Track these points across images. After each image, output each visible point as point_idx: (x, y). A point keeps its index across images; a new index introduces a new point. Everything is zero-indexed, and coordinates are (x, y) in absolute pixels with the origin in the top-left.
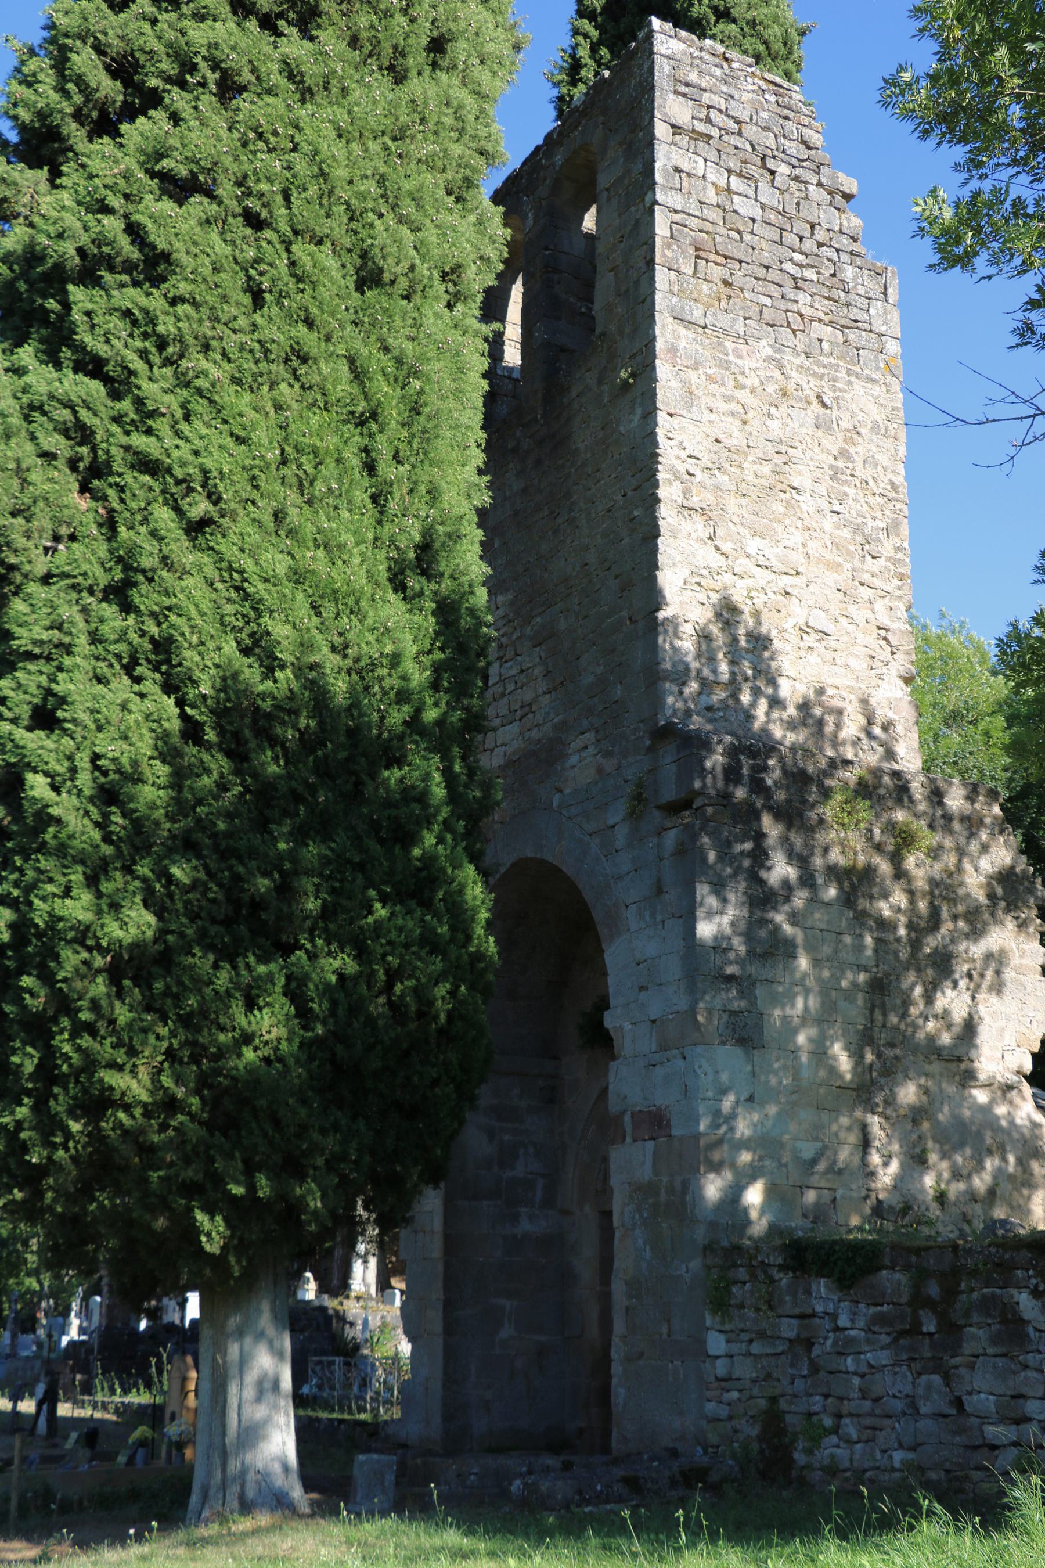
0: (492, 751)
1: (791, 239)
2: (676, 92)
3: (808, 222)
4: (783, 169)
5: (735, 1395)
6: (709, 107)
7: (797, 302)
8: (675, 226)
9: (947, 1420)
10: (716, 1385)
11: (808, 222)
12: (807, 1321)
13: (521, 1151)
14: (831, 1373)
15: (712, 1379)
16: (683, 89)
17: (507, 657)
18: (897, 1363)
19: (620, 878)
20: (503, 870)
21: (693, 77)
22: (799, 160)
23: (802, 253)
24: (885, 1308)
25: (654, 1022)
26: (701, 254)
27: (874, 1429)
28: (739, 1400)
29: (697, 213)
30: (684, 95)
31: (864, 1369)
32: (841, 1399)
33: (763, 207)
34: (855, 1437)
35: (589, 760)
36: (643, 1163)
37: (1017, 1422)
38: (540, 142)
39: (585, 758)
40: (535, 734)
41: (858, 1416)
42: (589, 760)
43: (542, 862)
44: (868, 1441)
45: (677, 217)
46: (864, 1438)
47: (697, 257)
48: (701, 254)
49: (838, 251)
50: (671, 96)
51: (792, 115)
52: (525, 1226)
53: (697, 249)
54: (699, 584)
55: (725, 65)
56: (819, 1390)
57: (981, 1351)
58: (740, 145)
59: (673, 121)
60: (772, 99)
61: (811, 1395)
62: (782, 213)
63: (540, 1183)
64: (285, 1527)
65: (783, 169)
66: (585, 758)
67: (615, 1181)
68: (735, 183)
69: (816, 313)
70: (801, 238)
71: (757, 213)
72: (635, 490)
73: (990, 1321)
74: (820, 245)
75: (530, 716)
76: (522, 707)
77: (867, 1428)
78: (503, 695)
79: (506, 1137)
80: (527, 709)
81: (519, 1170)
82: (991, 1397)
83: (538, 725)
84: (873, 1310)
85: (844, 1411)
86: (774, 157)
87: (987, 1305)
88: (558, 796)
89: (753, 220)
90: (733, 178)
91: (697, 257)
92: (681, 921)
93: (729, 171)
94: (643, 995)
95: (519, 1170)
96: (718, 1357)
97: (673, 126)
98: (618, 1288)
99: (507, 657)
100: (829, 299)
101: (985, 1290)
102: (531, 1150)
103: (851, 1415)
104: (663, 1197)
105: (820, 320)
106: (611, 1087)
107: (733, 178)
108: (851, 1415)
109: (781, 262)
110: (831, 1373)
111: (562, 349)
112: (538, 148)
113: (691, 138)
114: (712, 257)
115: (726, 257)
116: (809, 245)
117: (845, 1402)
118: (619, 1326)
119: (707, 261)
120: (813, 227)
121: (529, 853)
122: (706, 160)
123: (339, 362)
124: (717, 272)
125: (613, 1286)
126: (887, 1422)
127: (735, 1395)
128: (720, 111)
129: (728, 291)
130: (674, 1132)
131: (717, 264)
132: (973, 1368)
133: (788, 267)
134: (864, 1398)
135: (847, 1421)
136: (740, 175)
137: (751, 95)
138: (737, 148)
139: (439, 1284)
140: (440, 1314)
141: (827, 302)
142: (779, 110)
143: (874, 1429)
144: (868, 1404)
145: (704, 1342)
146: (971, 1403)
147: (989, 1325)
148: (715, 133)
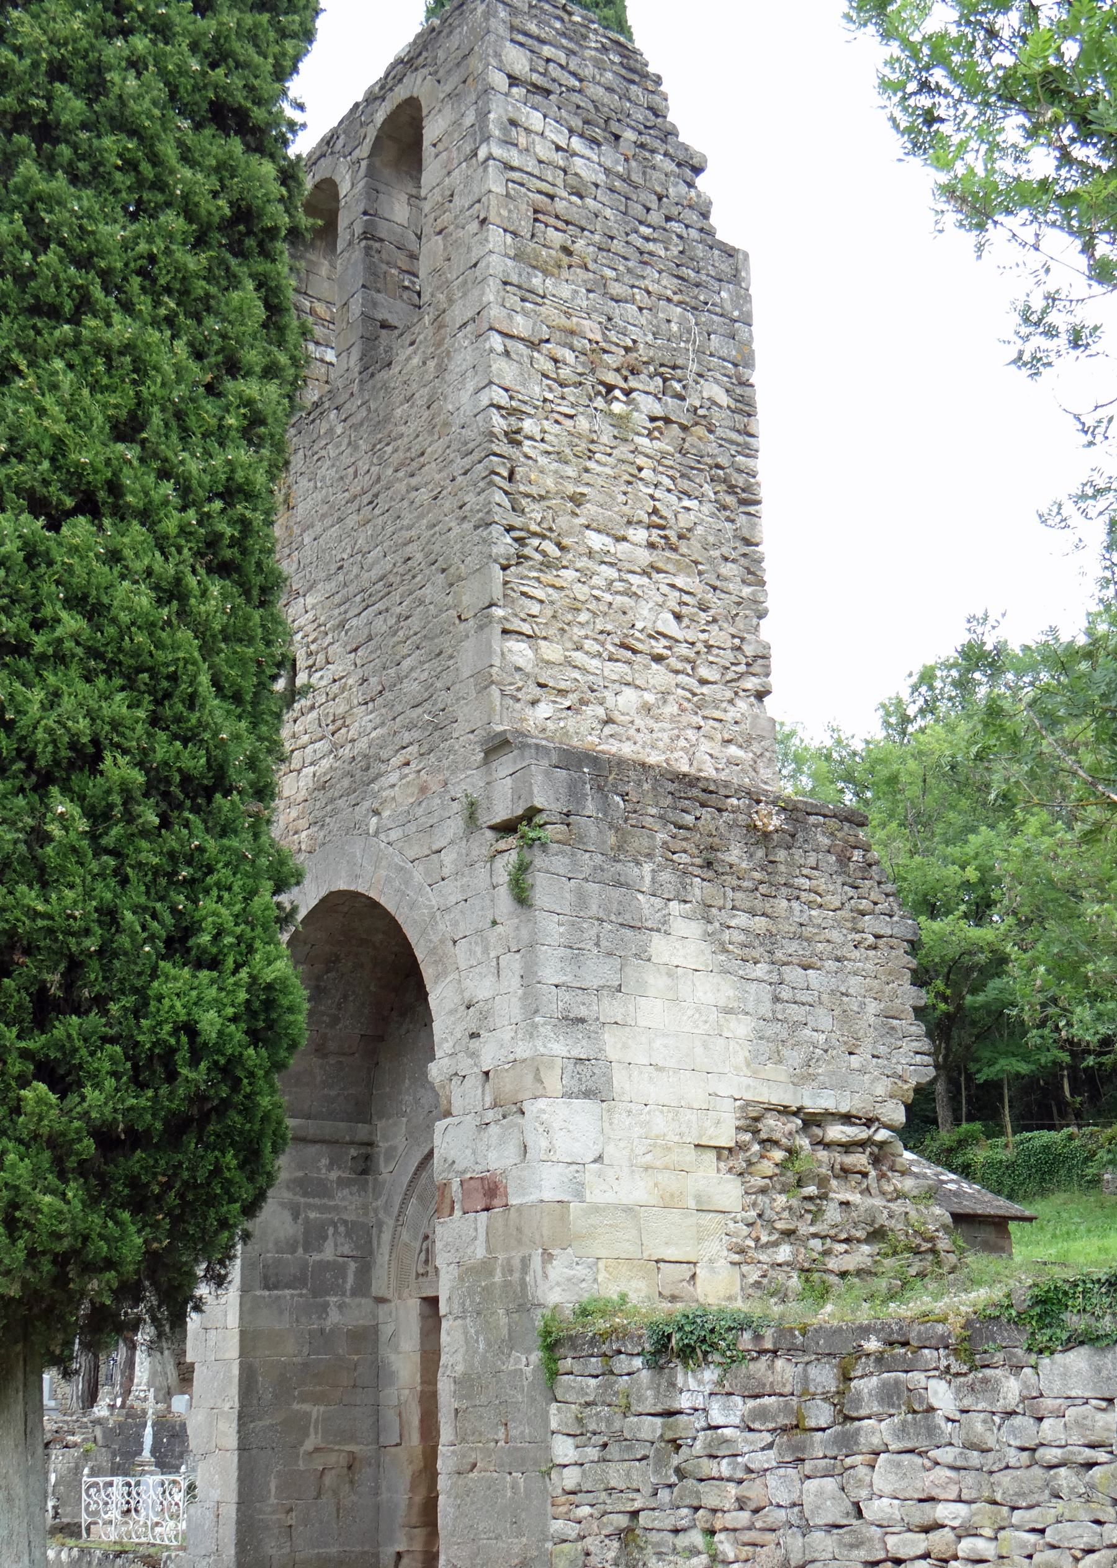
0: (299, 771)
1: (637, 210)
2: (512, 41)
3: (656, 193)
4: (629, 135)
5: (586, 1510)
6: (548, 60)
7: (644, 278)
8: (510, 185)
9: (841, 1531)
10: (563, 1499)
11: (656, 193)
12: (671, 1419)
13: (331, 1231)
14: (702, 1480)
15: (560, 1491)
16: (520, 38)
17: (318, 666)
18: (781, 1464)
19: (447, 909)
20: (301, 915)
21: (533, 28)
22: (646, 127)
23: (649, 226)
24: (766, 1400)
25: (487, 1073)
26: (540, 216)
27: (755, 1545)
28: (591, 1515)
29: (536, 172)
30: (521, 45)
31: (740, 1475)
32: (714, 1511)
33: (607, 171)
34: (731, 1556)
35: (412, 776)
36: (475, 1238)
37: (926, 1530)
38: (360, 98)
39: (406, 776)
40: (346, 752)
41: (735, 1530)
42: (412, 776)
43: (356, 895)
44: (747, 1561)
45: (516, 175)
46: (743, 1556)
47: (536, 220)
48: (540, 216)
49: (687, 226)
50: (508, 44)
51: (637, 78)
52: (334, 1317)
53: (536, 211)
54: (538, 579)
55: (566, 17)
56: (688, 1502)
57: (883, 1448)
58: (582, 104)
59: (508, 69)
60: (617, 59)
61: (678, 1508)
62: (626, 180)
63: (353, 1266)
64: (269, 1168)
65: (629, 135)
66: (406, 776)
67: (440, 1261)
68: (576, 143)
69: (662, 291)
70: (648, 210)
71: (601, 178)
72: (465, 474)
73: (892, 1411)
74: (668, 219)
75: (344, 730)
76: (333, 721)
77: (745, 1544)
78: (312, 708)
79: (312, 1215)
80: (340, 722)
81: (328, 1253)
82: (896, 1502)
83: (353, 741)
84: (752, 1403)
85: (718, 1526)
86: (619, 120)
87: (890, 1395)
88: (374, 820)
89: (597, 186)
90: (574, 139)
91: (536, 220)
92: (518, 956)
93: (571, 131)
94: (474, 1044)
95: (328, 1253)
96: (565, 1466)
97: (509, 76)
98: (445, 1387)
99: (318, 666)
100: (678, 277)
101: (886, 1375)
102: (342, 1229)
103: (726, 1529)
104: (498, 1278)
105: (669, 300)
106: (436, 1151)
107: (574, 139)
108: (726, 1529)
109: (627, 234)
110: (702, 1480)
111: (384, 325)
112: (357, 105)
113: (528, 91)
114: (552, 221)
115: (567, 223)
116: (655, 217)
117: (719, 1514)
118: (446, 1433)
119: (547, 226)
120: (660, 199)
121: (342, 886)
122: (545, 116)
123: (685, 1150)
124: (556, 238)
125: (440, 1385)
126: (769, 1537)
127: (586, 1510)
128: (561, 66)
129: (566, 260)
130: (513, 1201)
131: (557, 229)
132: (873, 1467)
133: (633, 237)
134: (741, 1509)
135: (719, 1537)
136: (581, 136)
137: (593, 53)
138: (578, 107)
139: (234, 1391)
140: (235, 1425)
141: (676, 281)
142: (623, 72)
143: (755, 1545)
144: (744, 1517)
145: (549, 1448)
146: (874, 1510)
147: (891, 1416)
148: (554, 87)
